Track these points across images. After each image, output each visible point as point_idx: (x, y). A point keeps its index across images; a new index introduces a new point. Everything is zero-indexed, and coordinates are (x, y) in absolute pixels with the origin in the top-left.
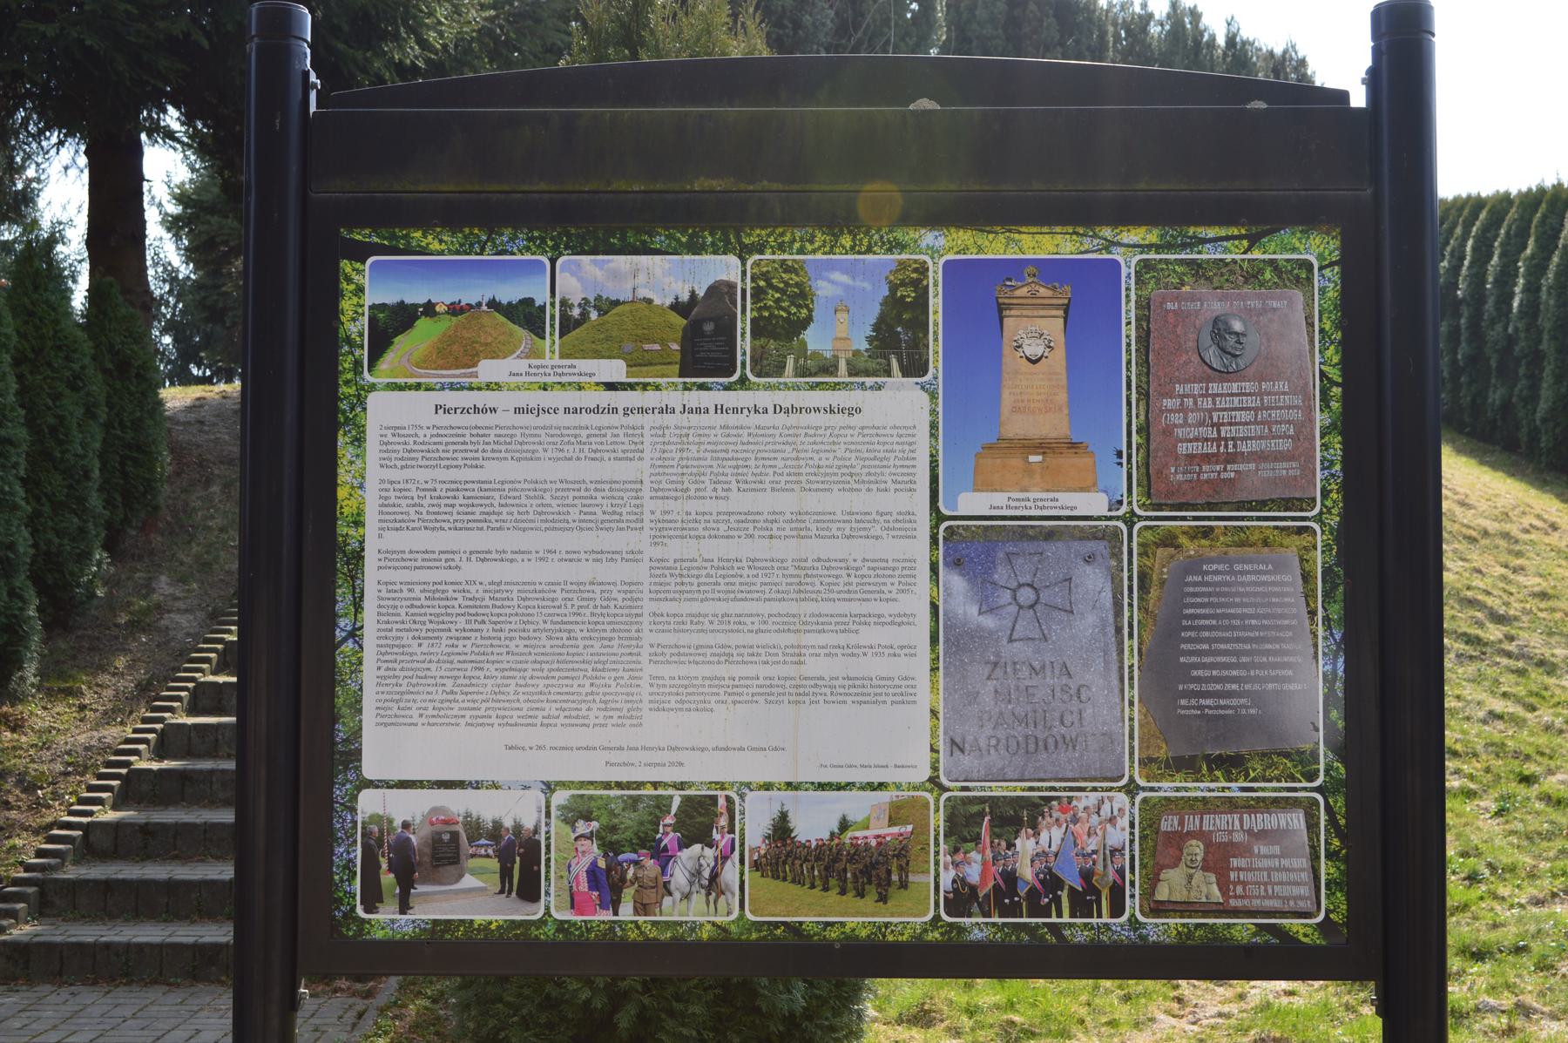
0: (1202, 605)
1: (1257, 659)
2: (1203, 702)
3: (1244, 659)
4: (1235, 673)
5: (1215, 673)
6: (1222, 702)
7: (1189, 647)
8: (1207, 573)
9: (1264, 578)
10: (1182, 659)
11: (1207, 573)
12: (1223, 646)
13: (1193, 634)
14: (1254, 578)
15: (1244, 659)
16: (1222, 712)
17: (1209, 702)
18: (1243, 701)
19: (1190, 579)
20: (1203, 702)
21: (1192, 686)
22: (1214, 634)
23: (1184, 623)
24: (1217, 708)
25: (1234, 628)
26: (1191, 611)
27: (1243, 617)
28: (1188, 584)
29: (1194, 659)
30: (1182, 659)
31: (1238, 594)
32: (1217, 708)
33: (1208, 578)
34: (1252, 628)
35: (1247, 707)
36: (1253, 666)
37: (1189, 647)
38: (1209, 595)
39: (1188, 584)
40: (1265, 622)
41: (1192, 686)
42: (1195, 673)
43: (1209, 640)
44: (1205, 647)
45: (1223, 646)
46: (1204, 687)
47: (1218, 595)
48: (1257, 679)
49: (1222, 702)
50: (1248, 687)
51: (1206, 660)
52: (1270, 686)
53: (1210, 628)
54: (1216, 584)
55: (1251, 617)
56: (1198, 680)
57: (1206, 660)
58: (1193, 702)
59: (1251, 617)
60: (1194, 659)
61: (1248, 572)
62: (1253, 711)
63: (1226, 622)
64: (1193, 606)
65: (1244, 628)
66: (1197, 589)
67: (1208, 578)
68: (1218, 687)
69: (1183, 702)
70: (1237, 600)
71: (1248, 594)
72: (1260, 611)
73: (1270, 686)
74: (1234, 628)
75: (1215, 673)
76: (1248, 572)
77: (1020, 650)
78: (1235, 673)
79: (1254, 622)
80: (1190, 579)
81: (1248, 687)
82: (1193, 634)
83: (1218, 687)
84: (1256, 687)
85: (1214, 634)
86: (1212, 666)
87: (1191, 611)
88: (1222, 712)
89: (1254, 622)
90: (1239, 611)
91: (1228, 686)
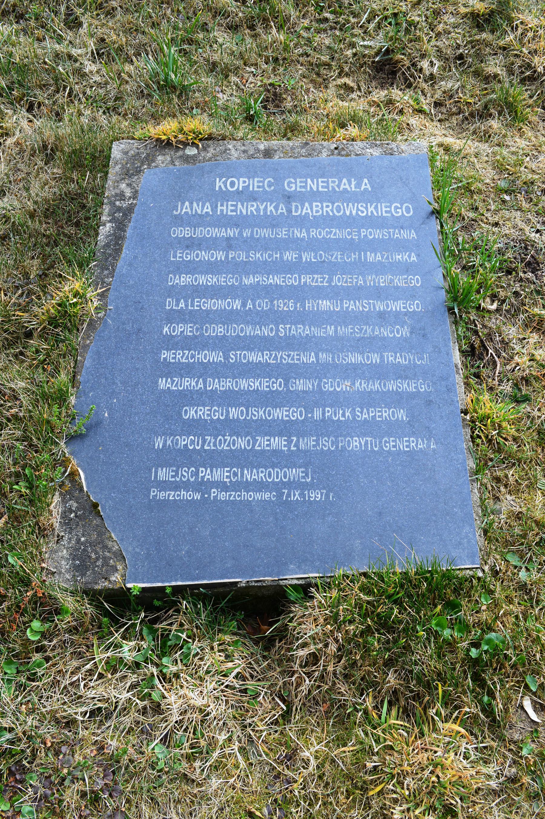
0: (212, 268)
1: (329, 386)
2: (205, 474)
3: (300, 385)
4: (279, 414)
5: (234, 413)
6: (249, 475)
7: (181, 356)
8: (225, 196)
9: (351, 210)
10: (163, 384)
11: (225, 196)
12: (254, 357)
13: (185, 329)
14: (328, 209)
15: (300, 385)
16: (245, 496)
17: (221, 474)
18: (295, 473)
19: (185, 208)
20: (205, 474)
21: (183, 441)
22: (236, 330)
23: (170, 304)
24: (237, 486)
25: (281, 318)
26: (184, 280)
27: (298, 293)
28: (180, 221)
29: (188, 383)
30: (163, 384)
31: (291, 243)
32: (237, 486)
33: (226, 208)
34: (318, 319)
35: (302, 487)
36: (321, 399)
37: (181, 356)
38: (229, 244)
39: (180, 221)
40: (350, 305)
41: (183, 441)
42: (402, 415)
43: (222, 344)
44: (215, 357)
45: (254, 357)
46: (210, 443)
47: (251, 244)
48: (324, 428)
49: (249, 475)
50: (307, 443)
51: (216, 385)
52: (356, 443)
53: (227, 317)
54: (238, 222)
55: (319, 293)
56: (196, 427)
57: (216, 385)
58: (186, 474)
59: (319, 293)
60: (188, 383)
61: (315, 196)
62: (316, 496)
63: (264, 305)
64: (191, 268)
65: (300, 318)
66: (201, 232)
67: (226, 208)
68: (242, 443)
69: (163, 474)
70: (289, 256)
71: (312, 245)
72: (338, 281)
73: (356, 443)
74: (281, 318)
75: (234, 413)
76: (315, 196)
77: (262, 748)
78: (279, 414)
79: (325, 304)
80: (185, 208)
81: (307, 443)
82: (185, 329)
83: (242, 443)
84: (326, 444)
85: (236, 330)
86: (230, 398)
87: (184, 280)
88: (245, 496)
89: (325, 304)
90: (292, 280)
91: (263, 443)
